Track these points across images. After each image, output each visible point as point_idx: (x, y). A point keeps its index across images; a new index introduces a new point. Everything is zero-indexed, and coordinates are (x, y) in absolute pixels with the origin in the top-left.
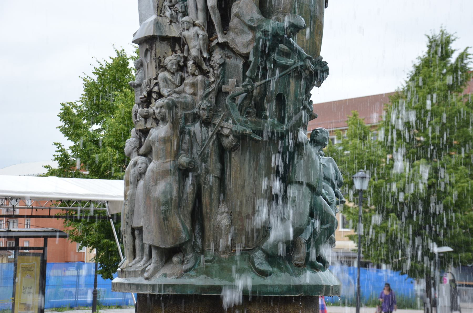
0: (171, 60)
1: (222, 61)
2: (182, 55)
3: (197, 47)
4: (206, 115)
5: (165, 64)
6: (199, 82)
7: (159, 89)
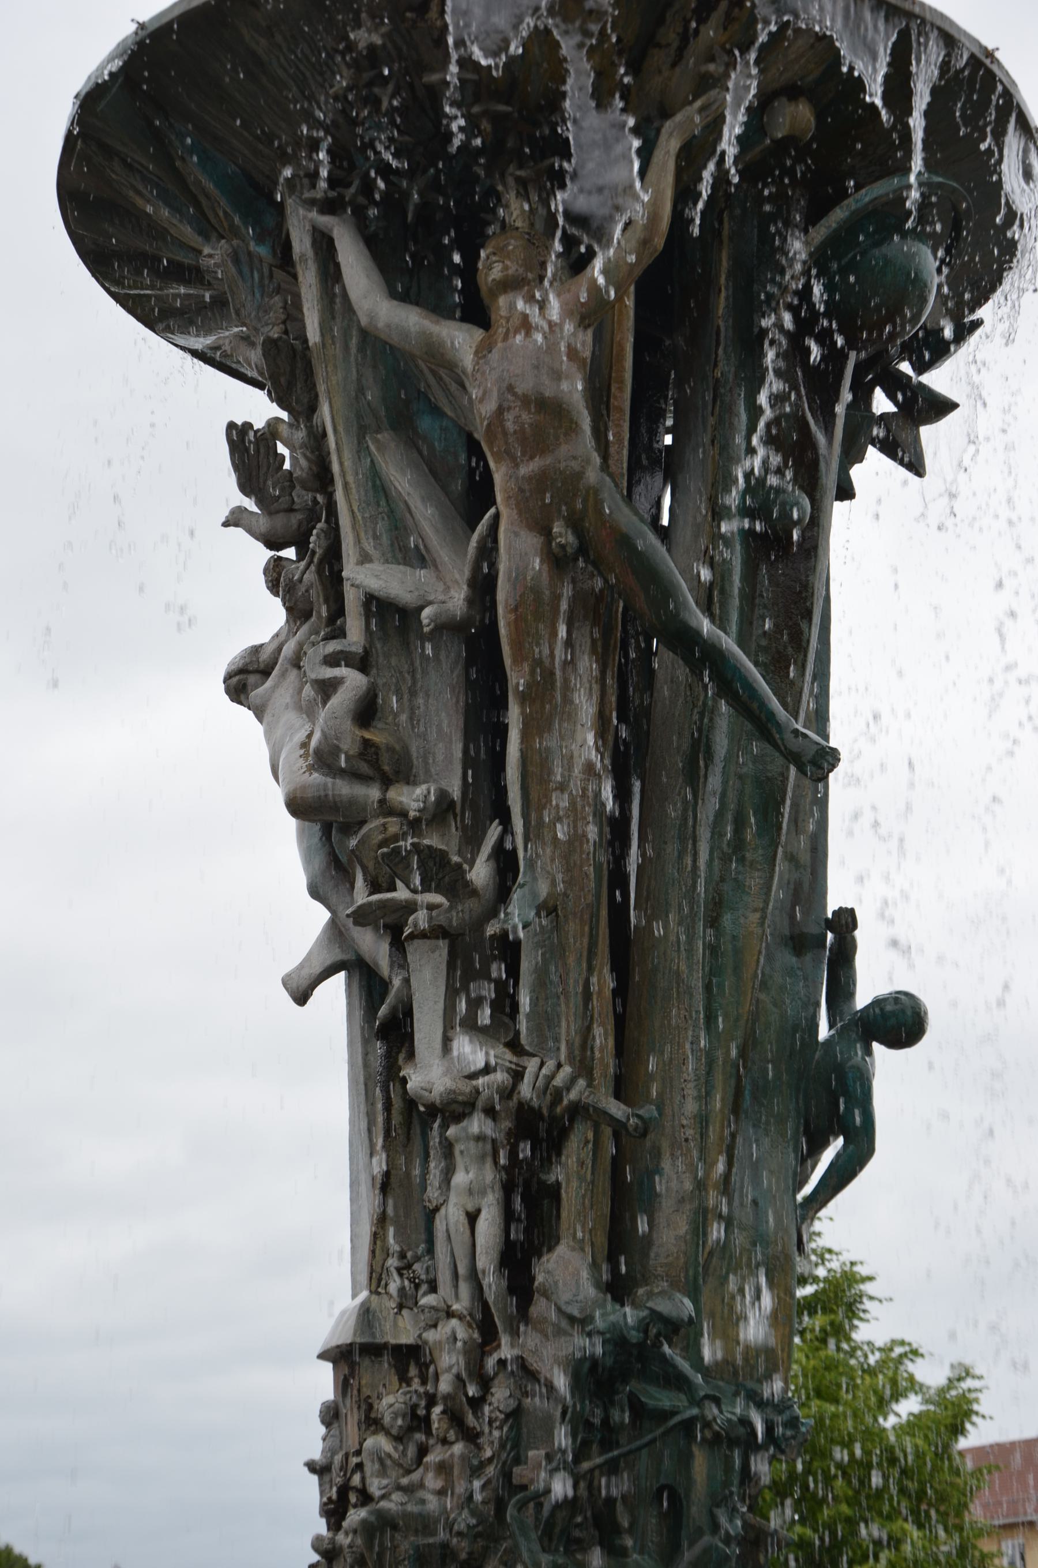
0: (391, 1405)
1: (512, 1404)
2: (421, 1390)
3: (454, 1371)
4: (467, 1550)
5: (380, 1416)
6: (456, 1460)
7: (363, 1479)
